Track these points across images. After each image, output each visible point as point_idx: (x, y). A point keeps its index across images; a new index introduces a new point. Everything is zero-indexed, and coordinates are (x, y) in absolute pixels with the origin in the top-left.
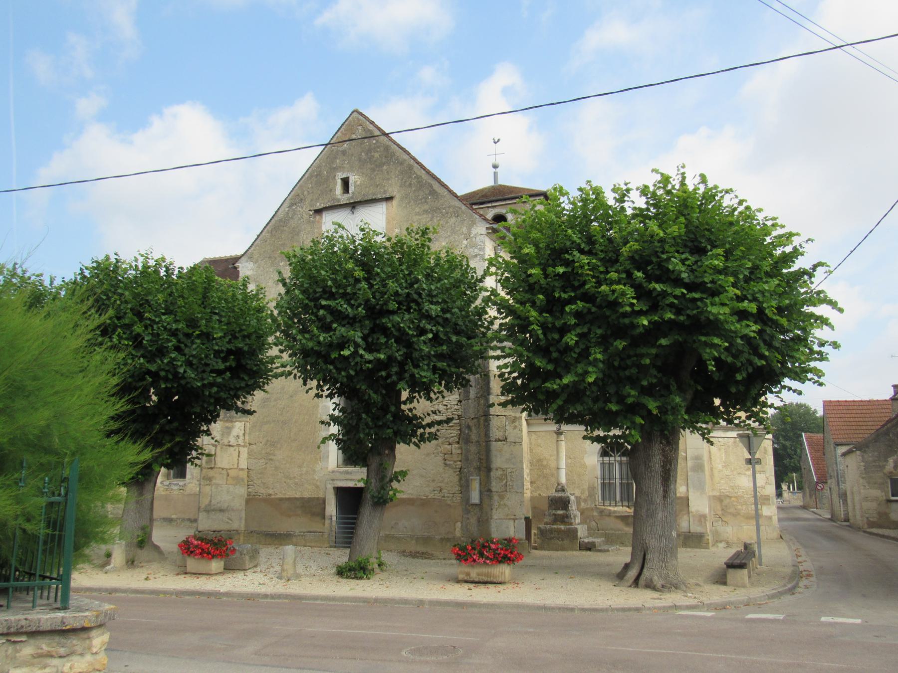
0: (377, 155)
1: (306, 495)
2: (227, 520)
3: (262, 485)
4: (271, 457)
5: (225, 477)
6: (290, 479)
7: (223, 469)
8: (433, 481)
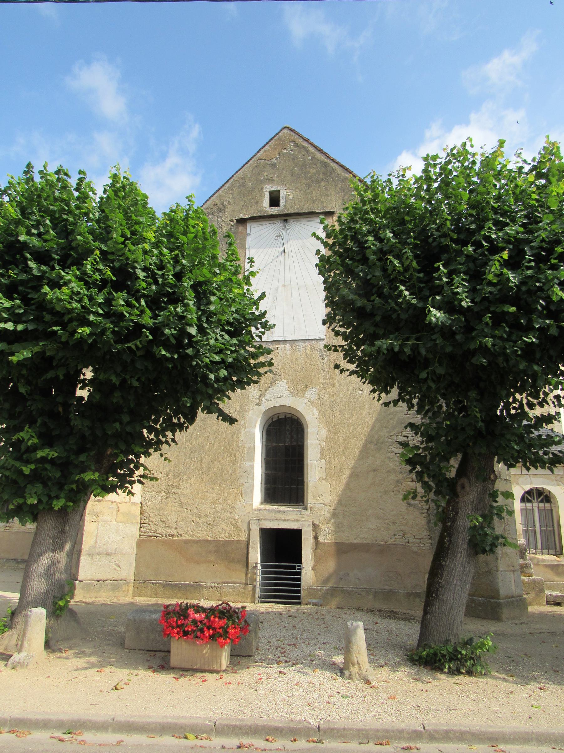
0: (313, 171)
1: (222, 537)
2: (115, 566)
3: (161, 523)
4: (174, 490)
5: (114, 513)
6: (200, 517)
7: (112, 502)
8: (394, 523)
